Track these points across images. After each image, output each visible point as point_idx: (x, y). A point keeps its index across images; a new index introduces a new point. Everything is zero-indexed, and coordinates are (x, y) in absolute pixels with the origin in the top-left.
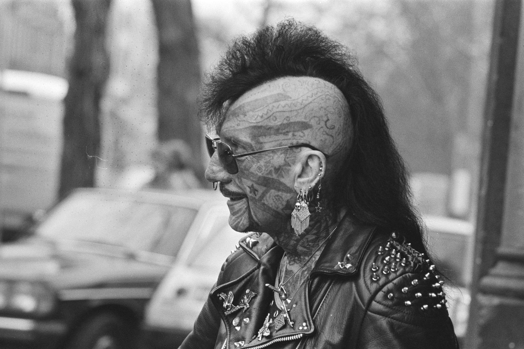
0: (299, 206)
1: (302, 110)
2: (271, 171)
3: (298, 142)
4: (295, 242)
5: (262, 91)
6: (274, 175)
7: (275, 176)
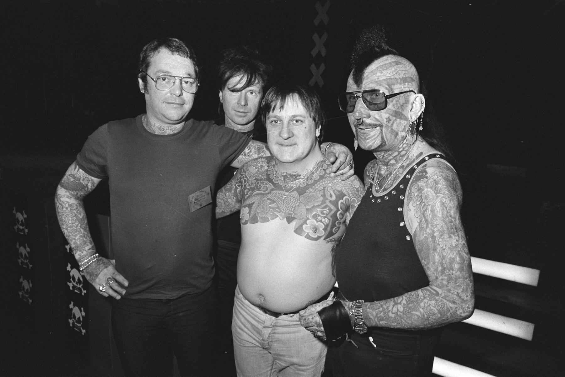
7: (400, 110)
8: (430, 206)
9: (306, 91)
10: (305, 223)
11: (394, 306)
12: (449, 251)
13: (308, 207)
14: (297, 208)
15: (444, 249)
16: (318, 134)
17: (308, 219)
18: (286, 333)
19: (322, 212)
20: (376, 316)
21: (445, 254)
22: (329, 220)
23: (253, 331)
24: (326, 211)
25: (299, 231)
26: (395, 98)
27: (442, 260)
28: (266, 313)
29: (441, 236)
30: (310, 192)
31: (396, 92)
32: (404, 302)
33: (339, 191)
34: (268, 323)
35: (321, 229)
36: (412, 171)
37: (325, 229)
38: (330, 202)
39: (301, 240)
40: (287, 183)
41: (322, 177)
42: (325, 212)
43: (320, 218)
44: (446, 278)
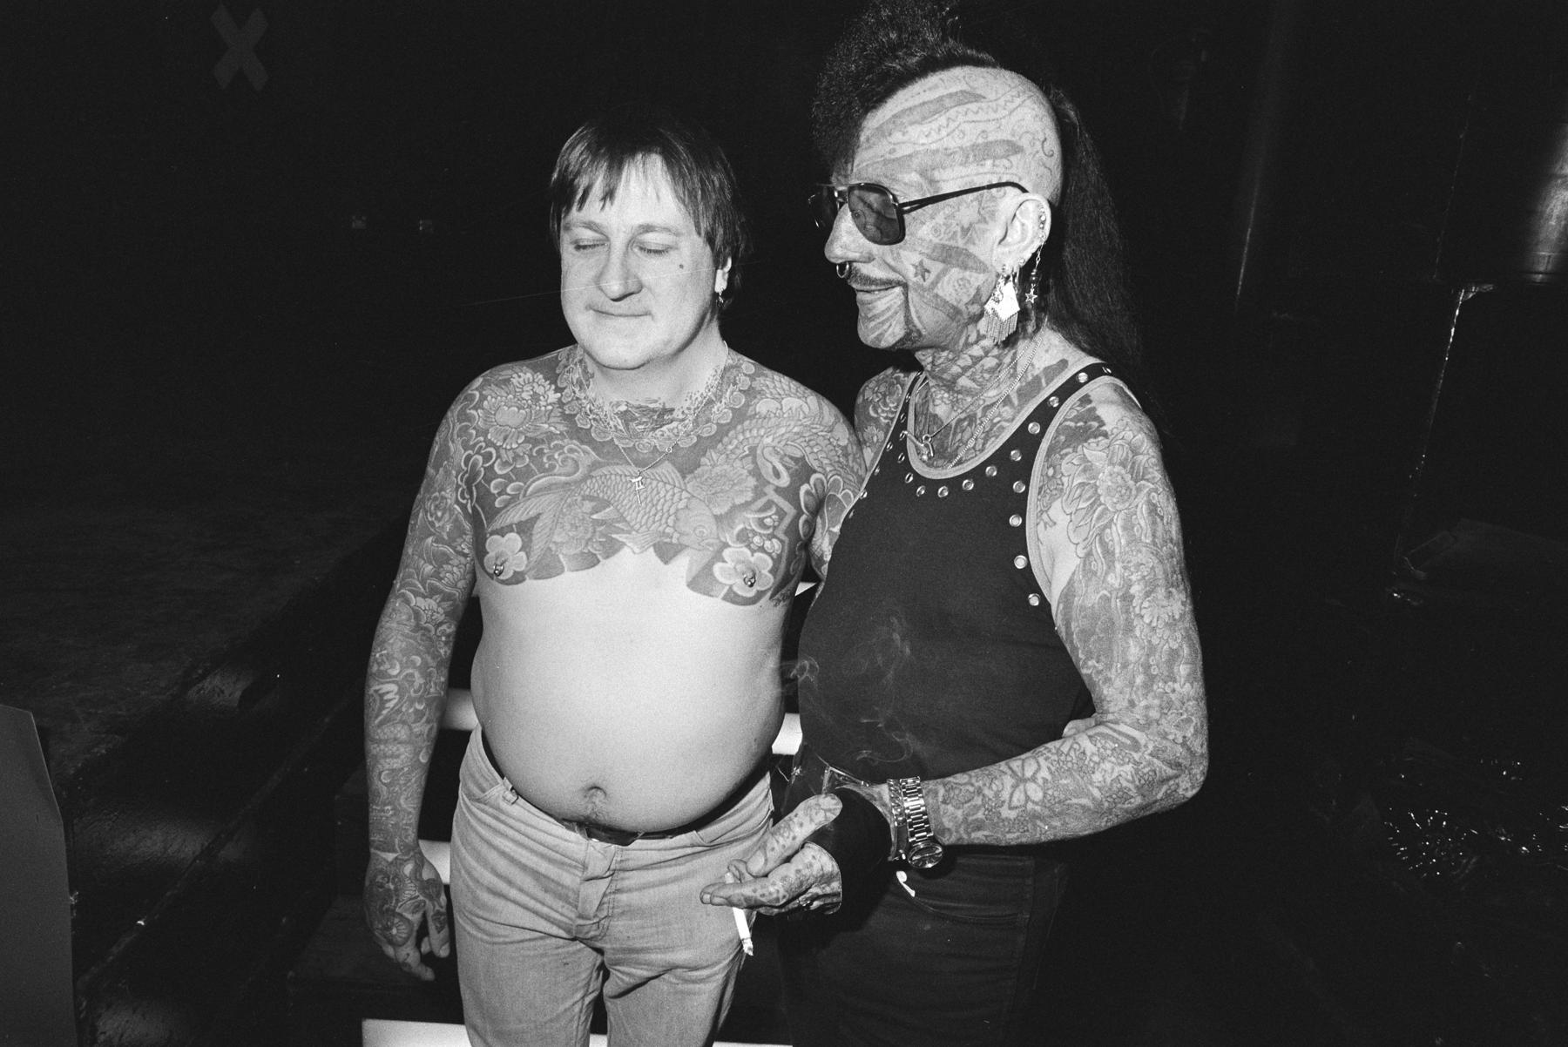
7: (960, 243)
8: (1122, 515)
9: (691, 149)
10: (718, 557)
11: (1015, 787)
12: (1167, 633)
13: (717, 511)
14: (682, 515)
15: (1154, 629)
16: (721, 285)
17: (726, 545)
18: (653, 885)
19: (761, 523)
20: (965, 820)
21: (1155, 641)
22: (782, 541)
23: (541, 894)
24: (770, 518)
25: (701, 582)
26: (943, 210)
27: (1148, 656)
28: (590, 836)
29: (1148, 594)
30: (714, 463)
31: (947, 189)
32: (1044, 773)
33: (796, 460)
34: (598, 867)
35: (765, 572)
36: (1044, 414)
37: (773, 571)
38: (778, 490)
39: (712, 607)
40: (638, 436)
41: (740, 416)
42: (768, 521)
43: (757, 539)
44: (1157, 702)
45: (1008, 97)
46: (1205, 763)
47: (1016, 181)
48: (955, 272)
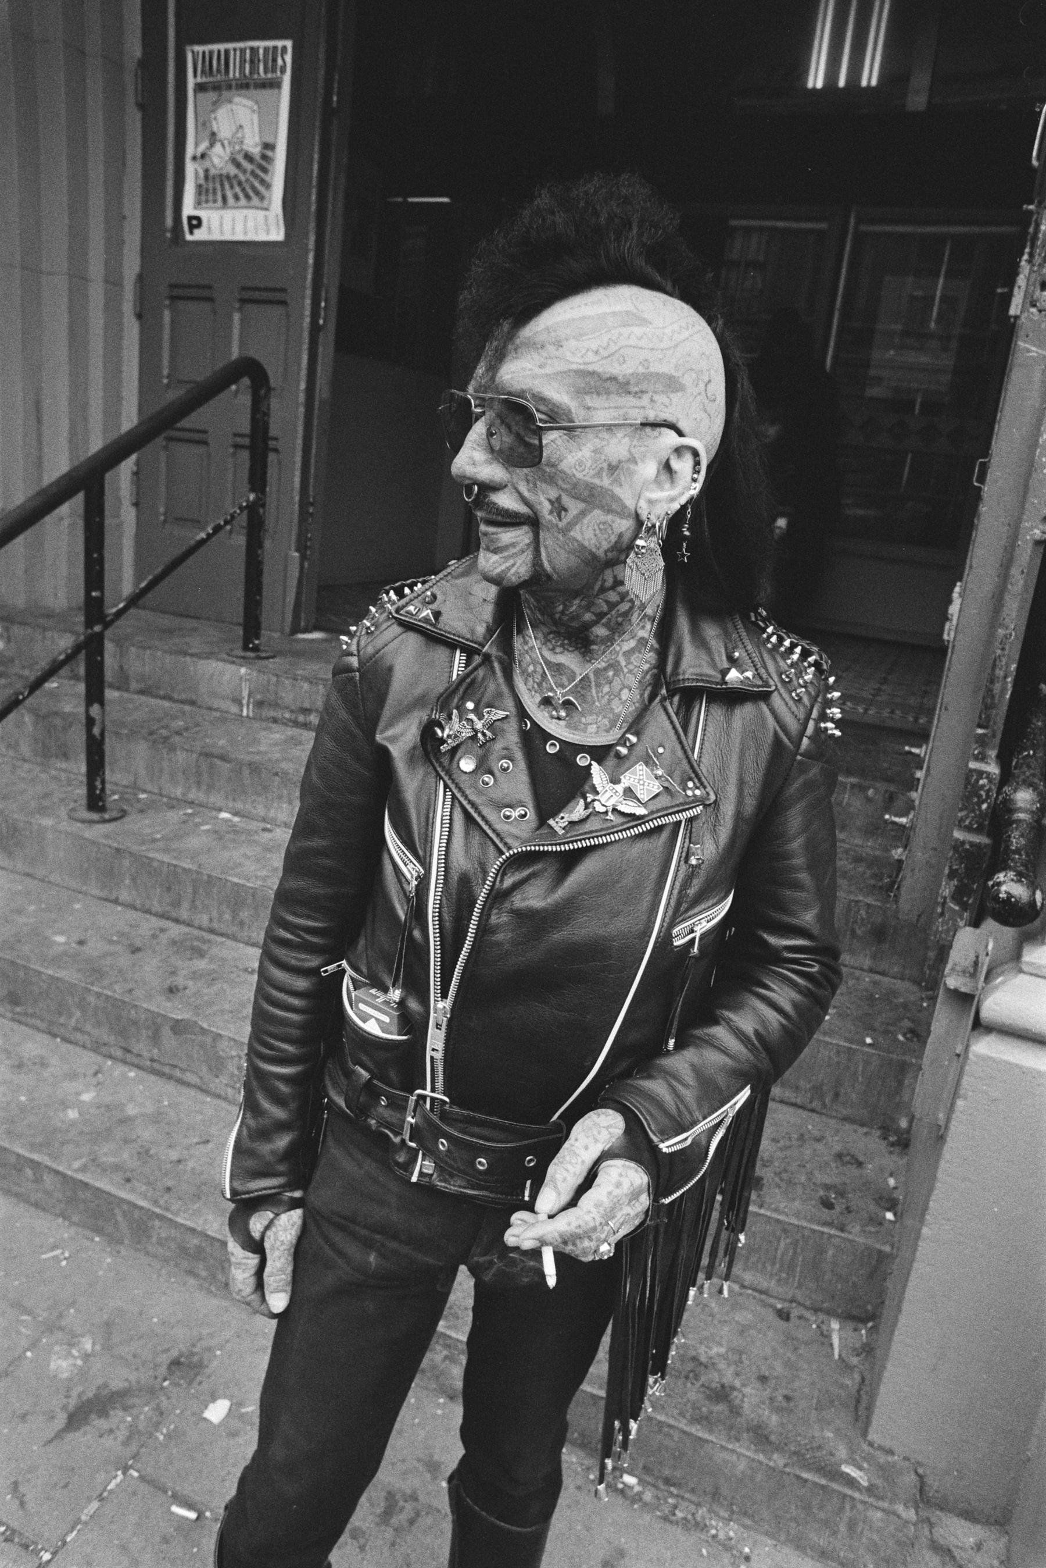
0: (643, 547)
1: (671, 352)
2: (602, 469)
3: (657, 416)
4: (594, 618)
5: (593, 303)
6: (605, 478)
7: (606, 482)
45: (676, 327)
46: (425, 1363)
47: (671, 419)
48: (597, 515)
